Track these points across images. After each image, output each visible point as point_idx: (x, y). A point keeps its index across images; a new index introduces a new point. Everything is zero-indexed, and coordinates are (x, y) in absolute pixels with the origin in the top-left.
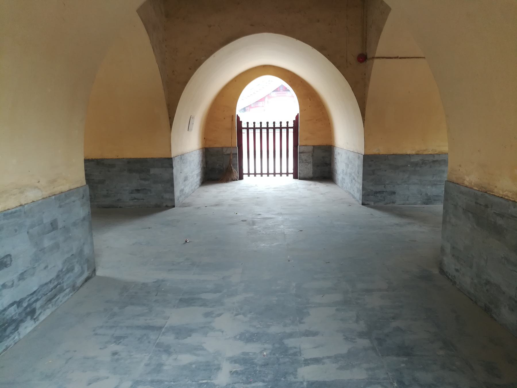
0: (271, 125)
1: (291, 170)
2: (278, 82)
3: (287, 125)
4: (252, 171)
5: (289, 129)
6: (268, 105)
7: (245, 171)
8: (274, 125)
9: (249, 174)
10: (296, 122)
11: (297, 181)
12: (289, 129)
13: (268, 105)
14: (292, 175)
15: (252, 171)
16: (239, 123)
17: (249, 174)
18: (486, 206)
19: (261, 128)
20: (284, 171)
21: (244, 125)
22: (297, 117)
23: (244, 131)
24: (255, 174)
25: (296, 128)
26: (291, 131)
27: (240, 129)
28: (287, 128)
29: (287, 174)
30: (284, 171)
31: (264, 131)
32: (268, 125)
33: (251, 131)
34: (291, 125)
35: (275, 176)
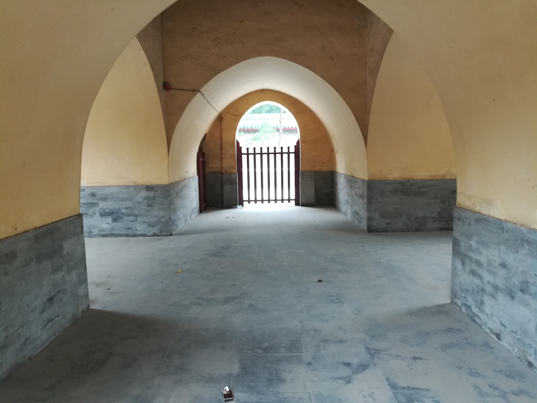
0: (272, 150)
1: (293, 196)
2: (289, 119)
3: (289, 150)
4: (252, 198)
5: (263, 155)
6: (267, 132)
7: (245, 197)
8: (248, 151)
9: (249, 201)
10: (297, 147)
11: (299, 208)
12: (263, 155)
13: (267, 132)
14: (294, 201)
15: (252, 198)
16: (239, 149)
17: (249, 201)
18: (412, 185)
19: (282, 153)
20: (286, 197)
21: (244, 151)
22: (298, 142)
23: (244, 157)
24: (256, 201)
25: (297, 153)
26: (292, 156)
27: (240, 154)
28: (289, 153)
29: (289, 200)
30: (286, 197)
31: (272, 157)
32: (248, 151)
33: (251, 157)
34: (292, 150)
35: (276, 202)
